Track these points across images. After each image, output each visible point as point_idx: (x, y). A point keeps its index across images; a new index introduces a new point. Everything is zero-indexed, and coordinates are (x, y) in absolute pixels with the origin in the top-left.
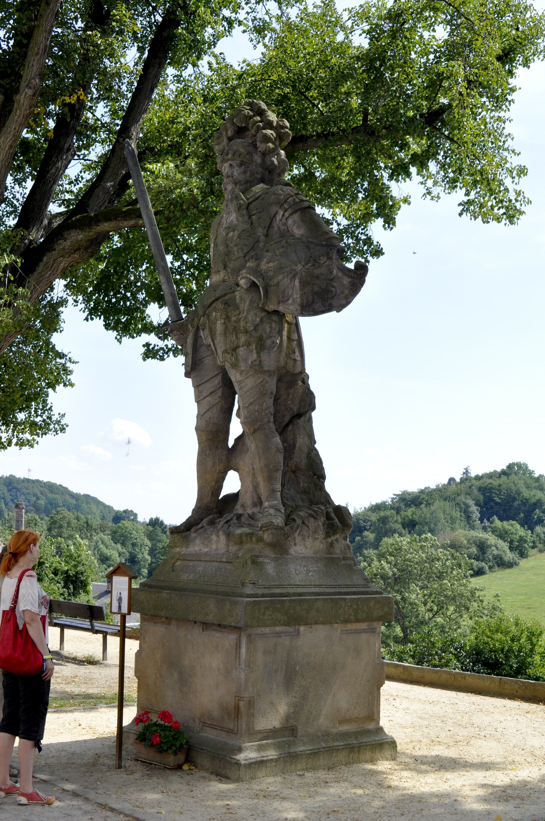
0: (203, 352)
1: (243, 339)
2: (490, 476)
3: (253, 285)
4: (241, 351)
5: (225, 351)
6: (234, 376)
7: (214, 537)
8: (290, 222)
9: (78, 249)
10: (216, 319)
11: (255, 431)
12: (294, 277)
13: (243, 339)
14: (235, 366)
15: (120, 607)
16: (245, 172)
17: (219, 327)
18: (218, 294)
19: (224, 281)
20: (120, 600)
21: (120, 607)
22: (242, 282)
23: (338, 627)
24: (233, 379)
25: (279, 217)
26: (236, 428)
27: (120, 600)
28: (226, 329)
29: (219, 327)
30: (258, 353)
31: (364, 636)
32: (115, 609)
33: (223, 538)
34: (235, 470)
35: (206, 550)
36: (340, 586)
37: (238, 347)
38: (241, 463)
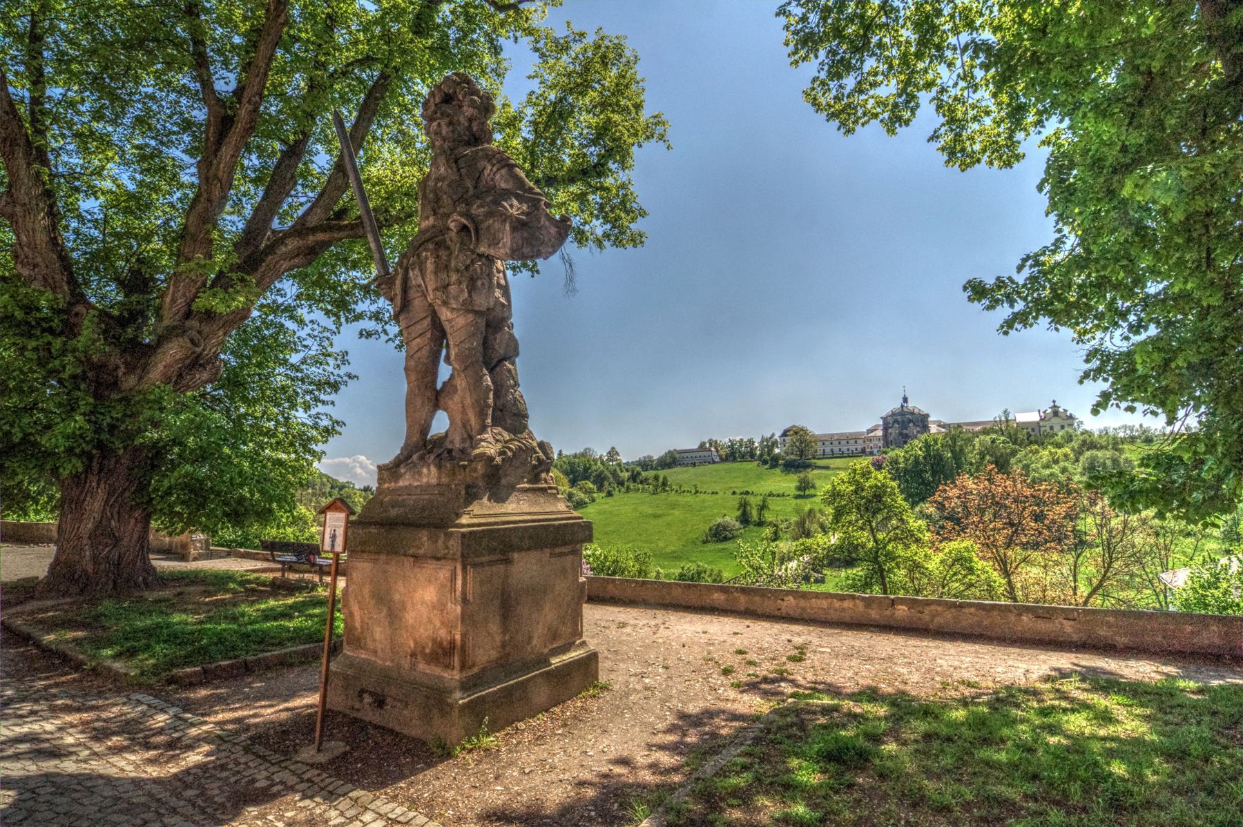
0: (412, 293)
1: (454, 277)
2: (575, 456)
3: (464, 228)
4: (453, 289)
5: (436, 289)
6: (445, 314)
7: (425, 470)
8: (498, 177)
9: (298, 255)
10: (426, 258)
11: (466, 369)
12: (505, 221)
13: (454, 277)
14: (445, 303)
15: (333, 546)
16: (453, 132)
17: (430, 266)
18: (428, 235)
19: (434, 226)
20: (334, 537)
21: (333, 546)
22: (452, 225)
23: (547, 551)
24: (443, 318)
25: (486, 172)
26: (444, 372)
27: (334, 537)
28: (436, 267)
29: (430, 266)
30: (470, 293)
31: (570, 558)
32: (327, 547)
33: (433, 469)
34: (446, 410)
35: (416, 484)
36: (547, 513)
37: (448, 285)
38: (450, 402)
